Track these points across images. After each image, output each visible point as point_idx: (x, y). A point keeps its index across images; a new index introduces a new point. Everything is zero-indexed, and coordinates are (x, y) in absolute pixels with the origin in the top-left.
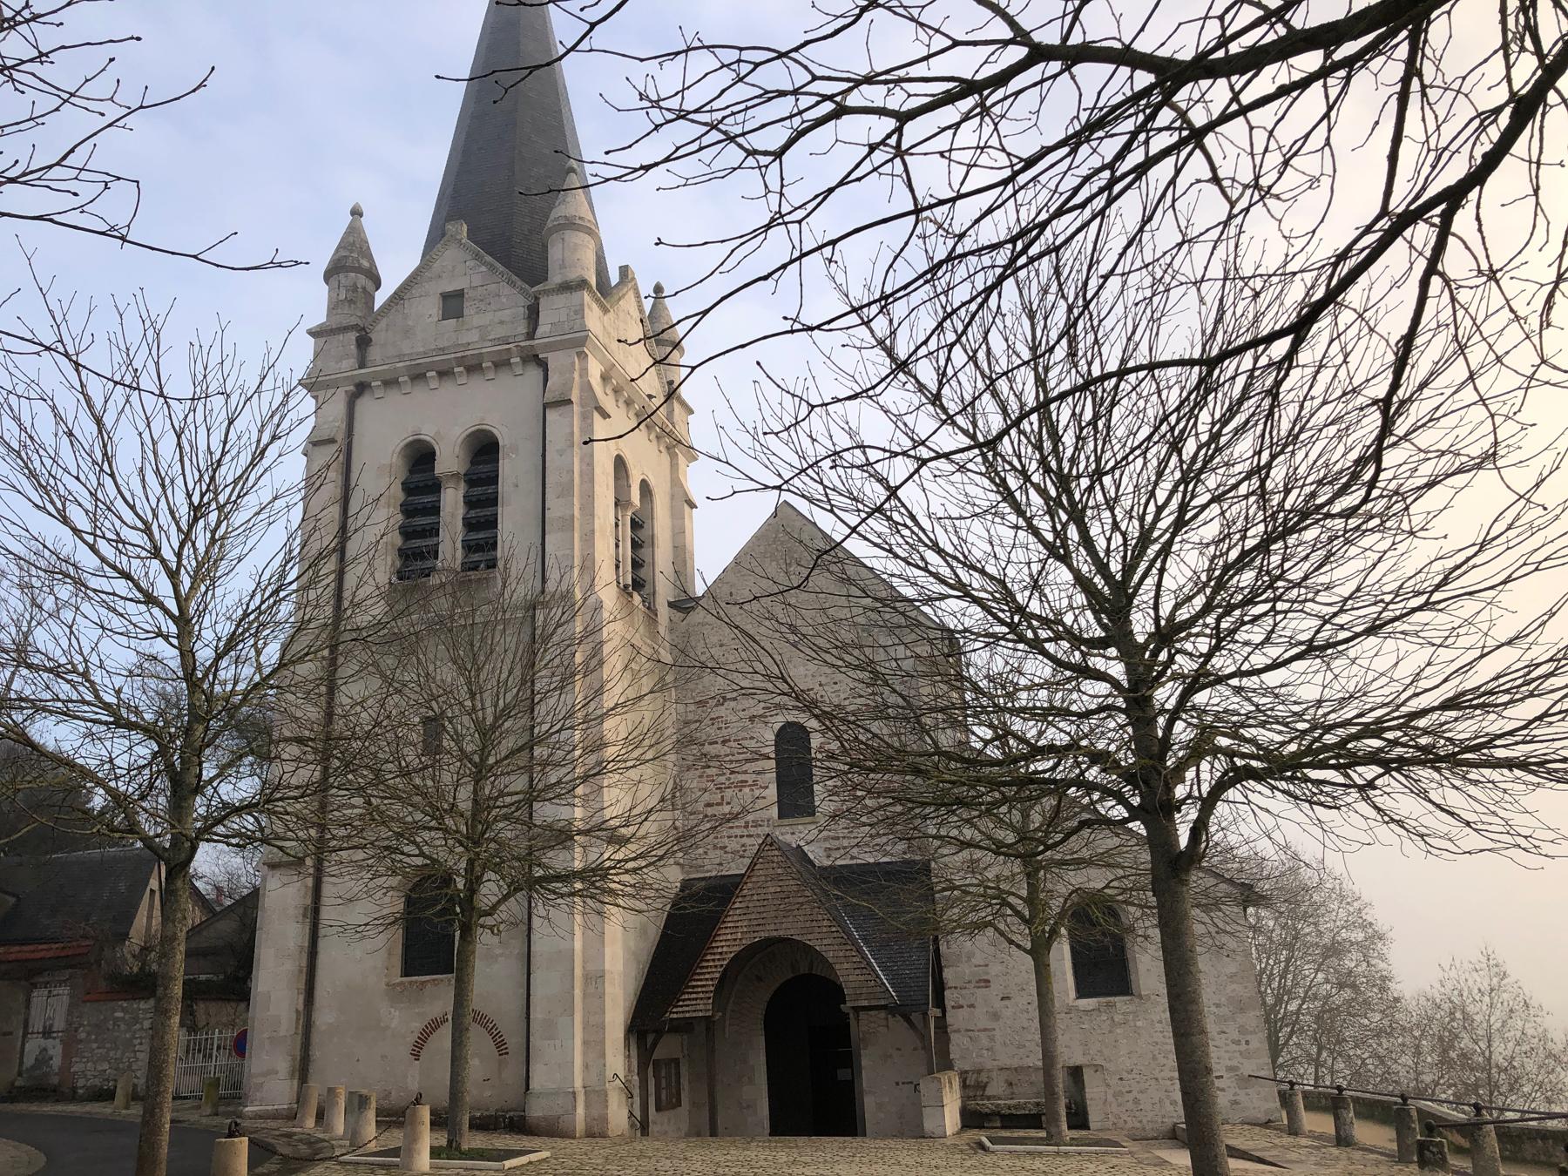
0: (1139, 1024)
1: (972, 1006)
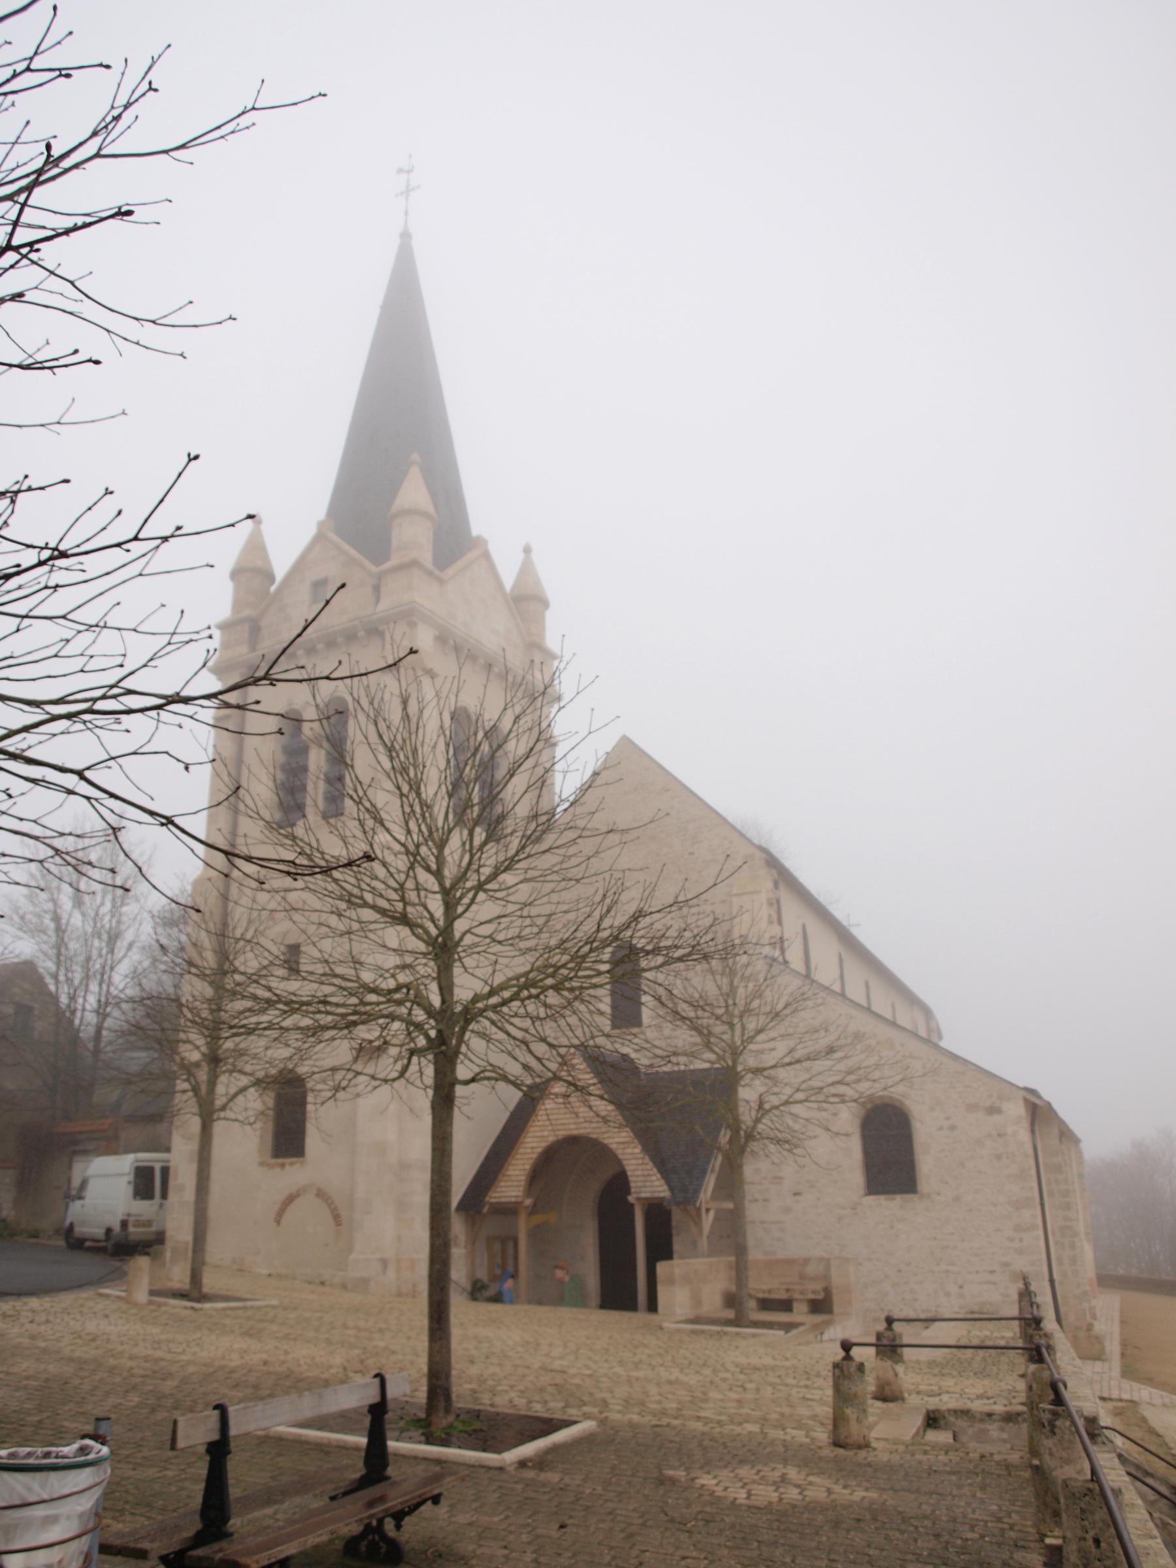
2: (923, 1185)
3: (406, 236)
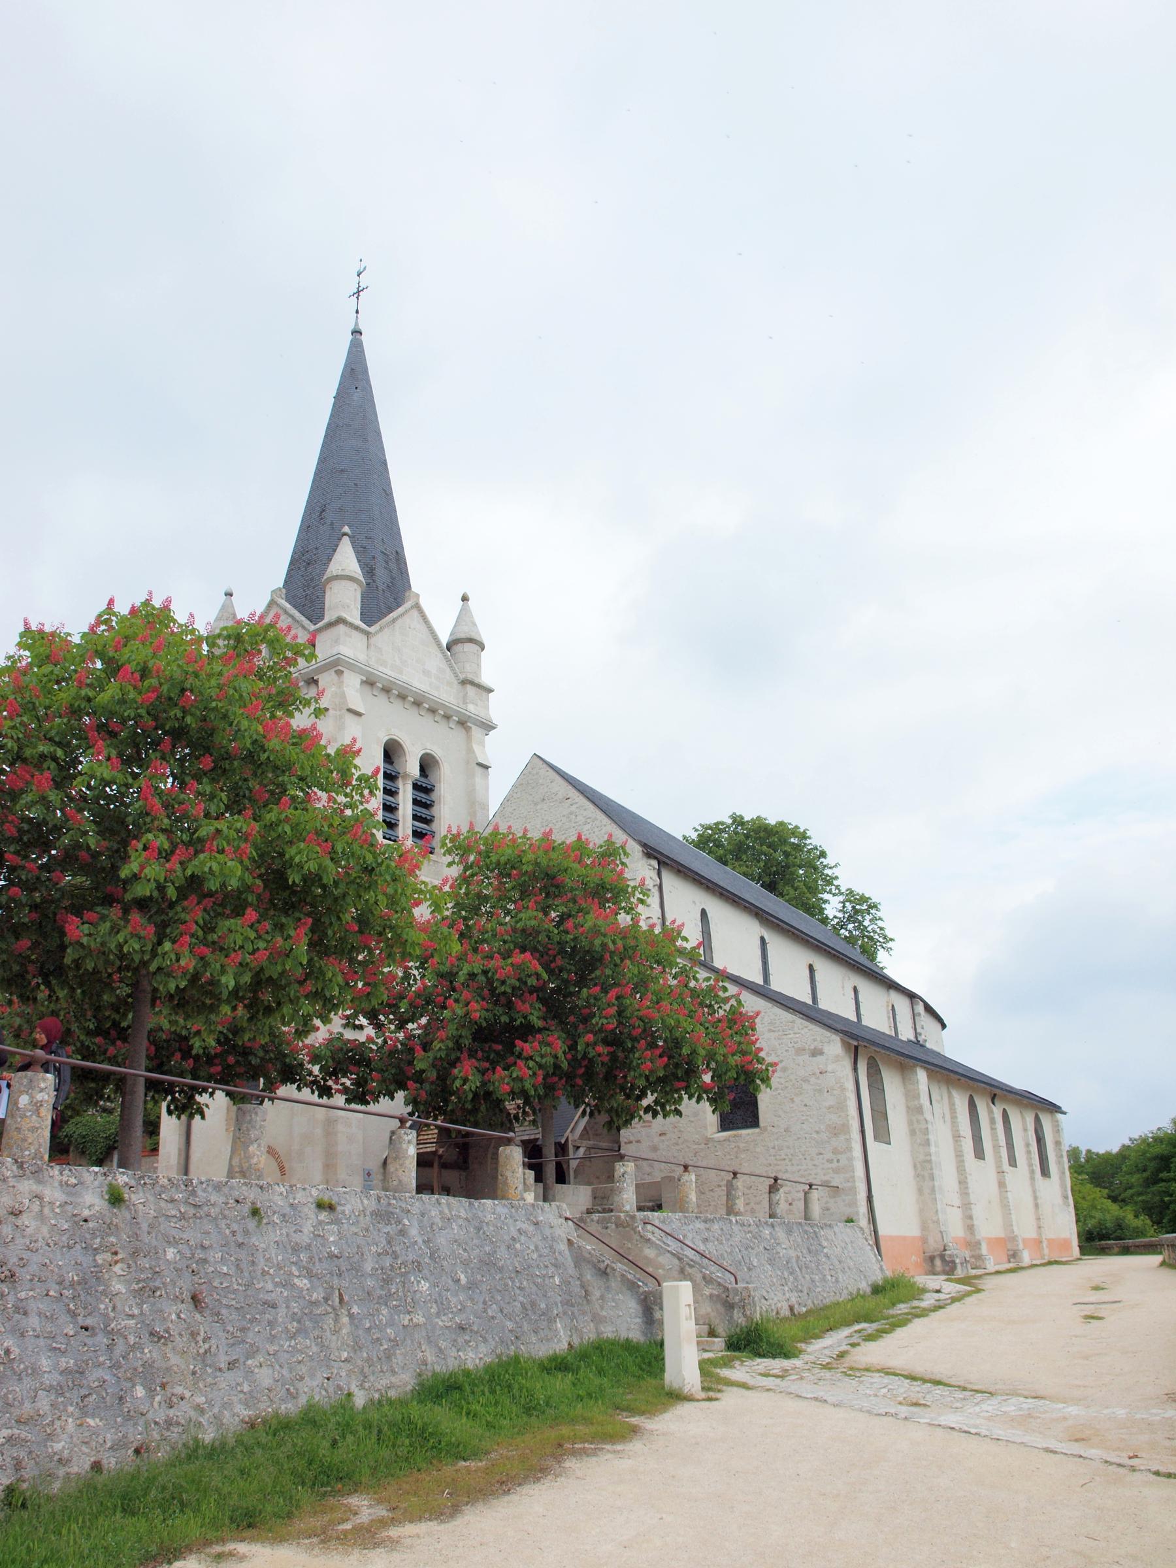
0: (758, 1150)
1: (638, 1141)
2: (762, 1123)
3: (357, 332)
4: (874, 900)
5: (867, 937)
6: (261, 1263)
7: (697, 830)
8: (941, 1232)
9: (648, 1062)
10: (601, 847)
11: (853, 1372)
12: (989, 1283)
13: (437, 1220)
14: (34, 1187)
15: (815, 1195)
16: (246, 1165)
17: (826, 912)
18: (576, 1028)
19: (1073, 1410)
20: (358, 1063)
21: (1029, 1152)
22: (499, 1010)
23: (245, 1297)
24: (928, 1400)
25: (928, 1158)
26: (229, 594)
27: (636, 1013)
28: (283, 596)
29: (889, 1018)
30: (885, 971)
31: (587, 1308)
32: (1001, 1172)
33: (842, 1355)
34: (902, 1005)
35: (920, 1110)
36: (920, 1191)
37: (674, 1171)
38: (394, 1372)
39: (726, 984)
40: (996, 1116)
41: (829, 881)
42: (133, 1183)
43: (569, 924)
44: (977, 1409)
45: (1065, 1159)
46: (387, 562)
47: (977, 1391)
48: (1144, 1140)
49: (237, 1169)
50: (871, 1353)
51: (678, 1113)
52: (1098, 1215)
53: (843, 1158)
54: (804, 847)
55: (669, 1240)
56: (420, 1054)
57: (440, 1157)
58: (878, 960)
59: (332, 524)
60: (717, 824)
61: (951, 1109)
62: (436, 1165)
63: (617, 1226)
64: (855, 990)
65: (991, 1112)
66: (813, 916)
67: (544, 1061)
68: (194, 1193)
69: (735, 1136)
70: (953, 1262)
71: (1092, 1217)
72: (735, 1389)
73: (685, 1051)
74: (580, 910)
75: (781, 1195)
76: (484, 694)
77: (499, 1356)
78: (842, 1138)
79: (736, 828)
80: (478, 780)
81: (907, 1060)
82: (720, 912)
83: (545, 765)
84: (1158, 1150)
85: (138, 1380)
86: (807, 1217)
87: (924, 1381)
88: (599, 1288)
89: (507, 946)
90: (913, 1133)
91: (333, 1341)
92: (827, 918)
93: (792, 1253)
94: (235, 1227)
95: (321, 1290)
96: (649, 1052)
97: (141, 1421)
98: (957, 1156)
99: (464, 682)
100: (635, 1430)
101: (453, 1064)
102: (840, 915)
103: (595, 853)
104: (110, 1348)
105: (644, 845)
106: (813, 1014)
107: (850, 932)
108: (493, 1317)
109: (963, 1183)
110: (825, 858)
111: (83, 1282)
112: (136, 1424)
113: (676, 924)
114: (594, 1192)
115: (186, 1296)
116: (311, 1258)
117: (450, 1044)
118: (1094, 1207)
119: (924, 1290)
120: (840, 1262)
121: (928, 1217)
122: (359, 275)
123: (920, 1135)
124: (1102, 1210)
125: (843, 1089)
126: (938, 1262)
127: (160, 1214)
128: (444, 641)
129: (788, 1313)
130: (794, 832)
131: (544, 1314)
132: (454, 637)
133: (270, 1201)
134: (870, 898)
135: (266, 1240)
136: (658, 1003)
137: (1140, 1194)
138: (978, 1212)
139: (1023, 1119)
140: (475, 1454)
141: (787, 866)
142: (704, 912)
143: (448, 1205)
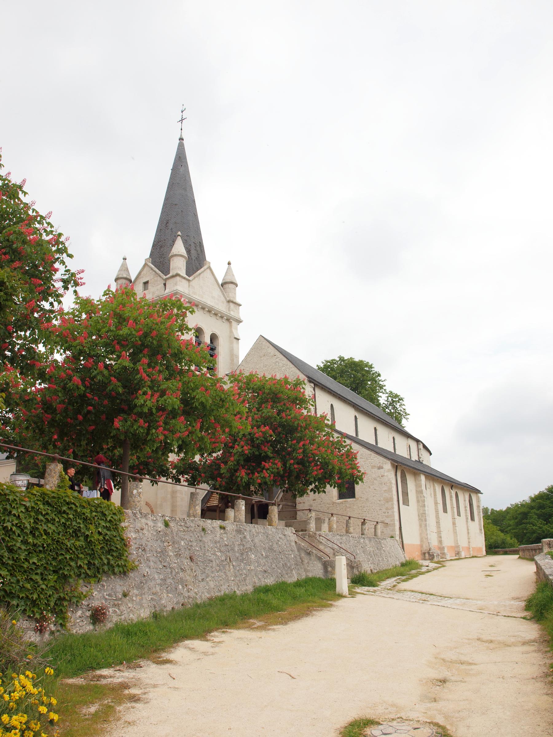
0: (354, 507)
1: (304, 503)
3: (181, 139)
4: (401, 396)
5: (398, 413)
6: (207, 547)
7: (323, 363)
8: (429, 543)
9: (315, 472)
10: (295, 381)
11: (399, 591)
12: (448, 564)
13: (255, 533)
14: (145, 521)
15: (379, 526)
16: (195, 513)
17: (380, 401)
18: (285, 457)
19: (479, 602)
20: (192, 469)
21: (466, 510)
22: (254, 450)
23: (204, 558)
24: (429, 599)
25: (424, 512)
26: (125, 259)
27: (311, 452)
28: (151, 262)
29: (407, 450)
30: (405, 428)
31: (302, 566)
32: (454, 518)
33: (394, 586)
34: (413, 445)
35: (421, 492)
36: (421, 526)
37: (319, 515)
38: (247, 585)
39: (345, 440)
40: (453, 495)
41: (381, 387)
42: (170, 520)
43: (283, 414)
44: (446, 602)
45: (481, 513)
46: (196, 247)
47: (446, 597)
48: (517, 505)
49: (192, 515)
50: (404, 586)
51: (325, 492)
52: (495, 538)
53: (390, 512)
54: (371, 372)
55: (329, 542)
56: (223, 466)
57: (220, 507)
58: (402, 423)
59: (172, 229)
60: (333, 360)
61: (434, 492)
62: (218, 511)
63: (309, 537)
64: (394, 438)
65: (450, 493)
66: (373, 403)
67: (273, 470)
68: (186, 523)
69: (345, 501)
70: (433, 555)
71: (491, 538)
72: (360, 595)
73: (330, 467)
74: (288, 409)
75: (366, 526)
76: (238, 307)
77: (277, 582)
78: (390, 503)
79: (341, 362)
80: (235, 345)
81: (417, 471)
82: (340, 407)
83: (265, 340)
84: (523, 510)
85: (179, 583)
86: (375, 534)
87: (426, 594)
88: (307, 559)
89: (258, 423)
90: (418, 501)
91: (229, 574)
92: (380, 404)
93: (371, 549)
94: (198, 534)
95: (224, 556)
96: (315, 468)
97: (182, 596)
98: (436, 511)
99: (229, 302)
100: (331, 605)
101: (236, 471)
102: (386, 403)
103: (292, 383)
104: (171, 572)
105: (308, 377)
106: (376, 450)
107: (390, 410)
108: (274, 568)
109: (438, 523)
110: (380, 376)
111: (162, 552)
112: (181, 597)
113: (325, 414)
114: (286, 523)
115: (188, 557)
116: (220, 545)
117: (236, 463)
118: (493, 534)
119: (422, 566)
120: (389, 553)
121: (423, 538)
122: (182, 112)
123: (421, 502)
124: (496, 536)
125: (391, 483)
126: (427, 555)
127: (179, 530)
128: (220, 282)
129: (370, 572)
130: (367, 365)
131: (289, 568)
132: (224, 281)
133: (206, 526)
134: (399, 396)
135: (207, 539)
136: (319, 448)
137: (513, 529)
138: (443, 535)
139: (464, 496)
140: (282, 610)
141: (363, 381)
142: (332, 405)
143: (257, 528)
